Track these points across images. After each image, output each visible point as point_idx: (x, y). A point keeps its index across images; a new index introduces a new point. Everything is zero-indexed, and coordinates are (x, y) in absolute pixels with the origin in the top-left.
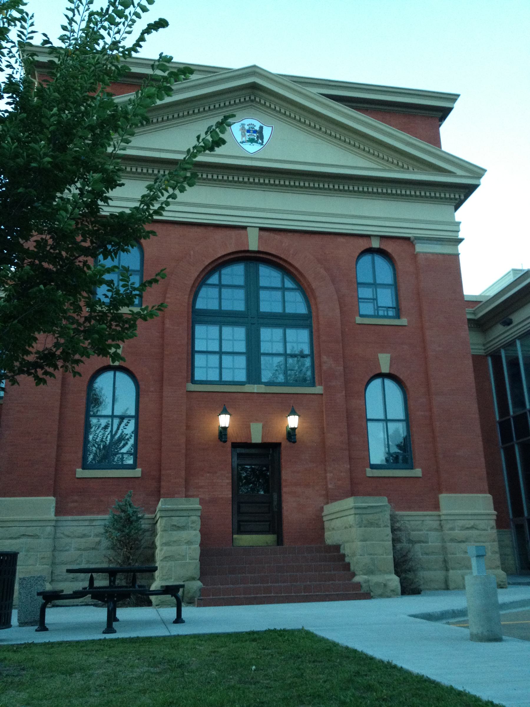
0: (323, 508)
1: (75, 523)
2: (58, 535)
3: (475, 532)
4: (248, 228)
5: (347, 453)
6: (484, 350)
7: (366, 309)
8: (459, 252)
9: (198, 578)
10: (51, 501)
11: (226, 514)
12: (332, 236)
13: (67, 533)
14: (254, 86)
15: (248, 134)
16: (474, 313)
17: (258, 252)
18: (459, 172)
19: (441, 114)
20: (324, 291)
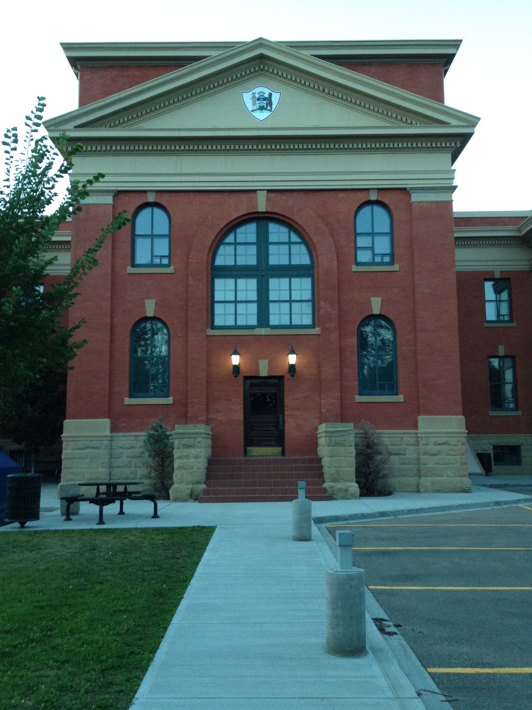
0: (317, 427)
1: (126, 438)
2: (113, 447)
3: (447, 447)
4: (258, 191)
5: (338, 383)
6: (530, 265)
7: (363, 256)
8: (453, 199)
9: (203, 482)
10: (106, 422)
11: (237, 434)
12: (333, 192)
13: (119, 445)
14: (262, 57)
15: (259, 102)
16: (519, 231)
17: (266, 212)
18: (453, 122)
19: (445, 60)
20: (325, 245)
